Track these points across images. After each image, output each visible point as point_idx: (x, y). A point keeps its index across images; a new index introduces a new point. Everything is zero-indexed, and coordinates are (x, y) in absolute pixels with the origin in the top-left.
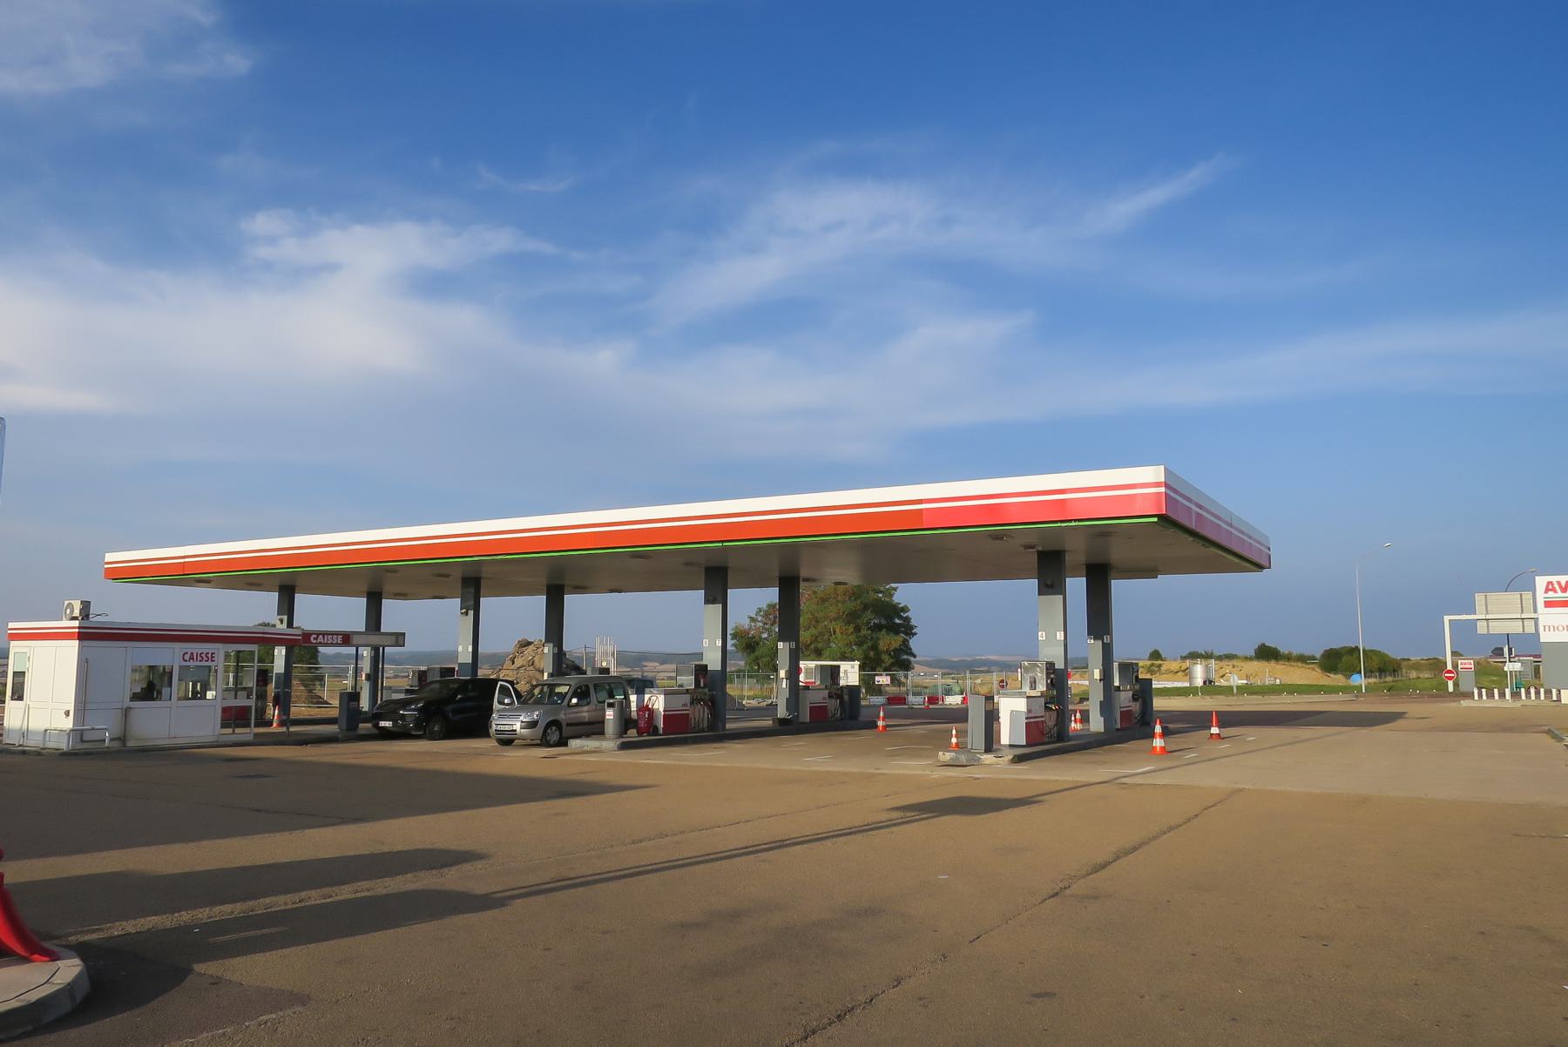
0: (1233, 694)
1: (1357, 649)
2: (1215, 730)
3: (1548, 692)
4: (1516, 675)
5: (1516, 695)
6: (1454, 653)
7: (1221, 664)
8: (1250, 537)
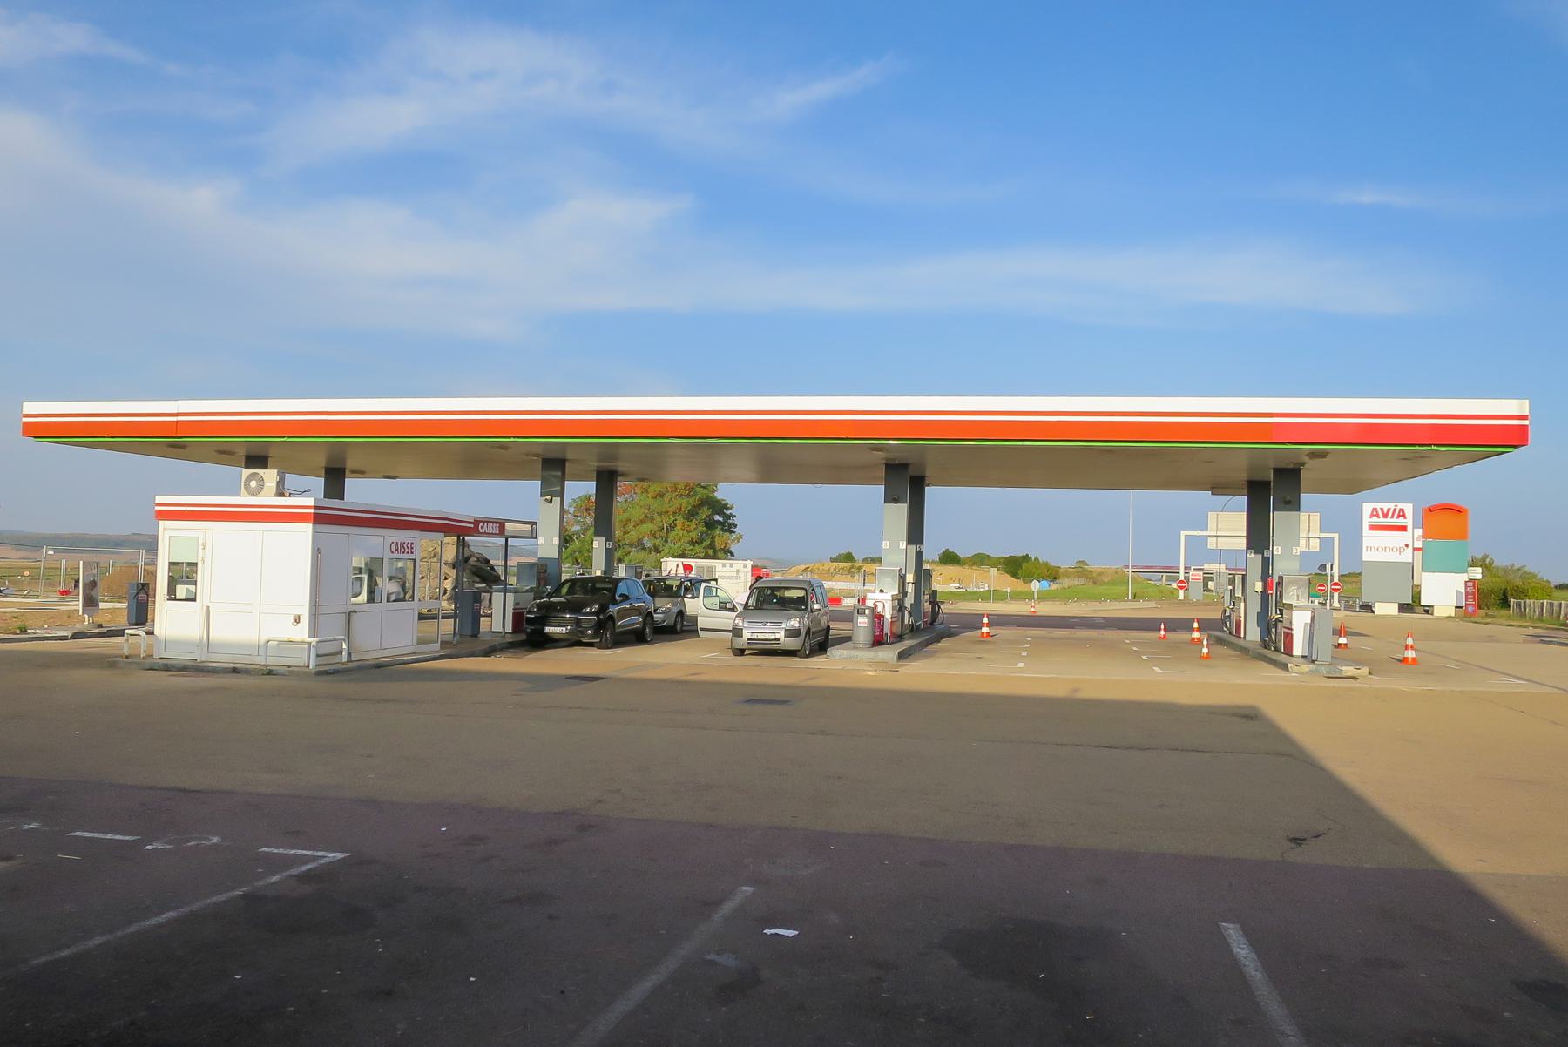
2: (985, 630)
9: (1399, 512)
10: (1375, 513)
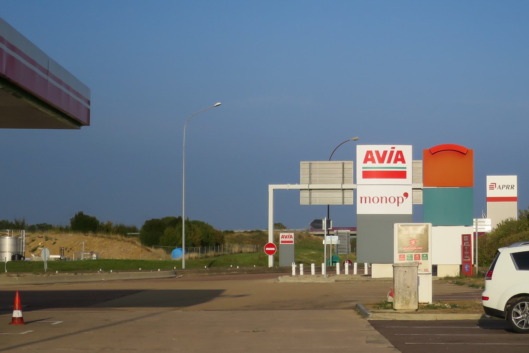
0: (43, 272)
1: (180, 219)
2: (17, 314)
3: (361, 267)
4: (333, 250)
5: (331, 270)
6: (278, 226)
7: (33, 236)
8: (68, 88)
9: (397, 156)
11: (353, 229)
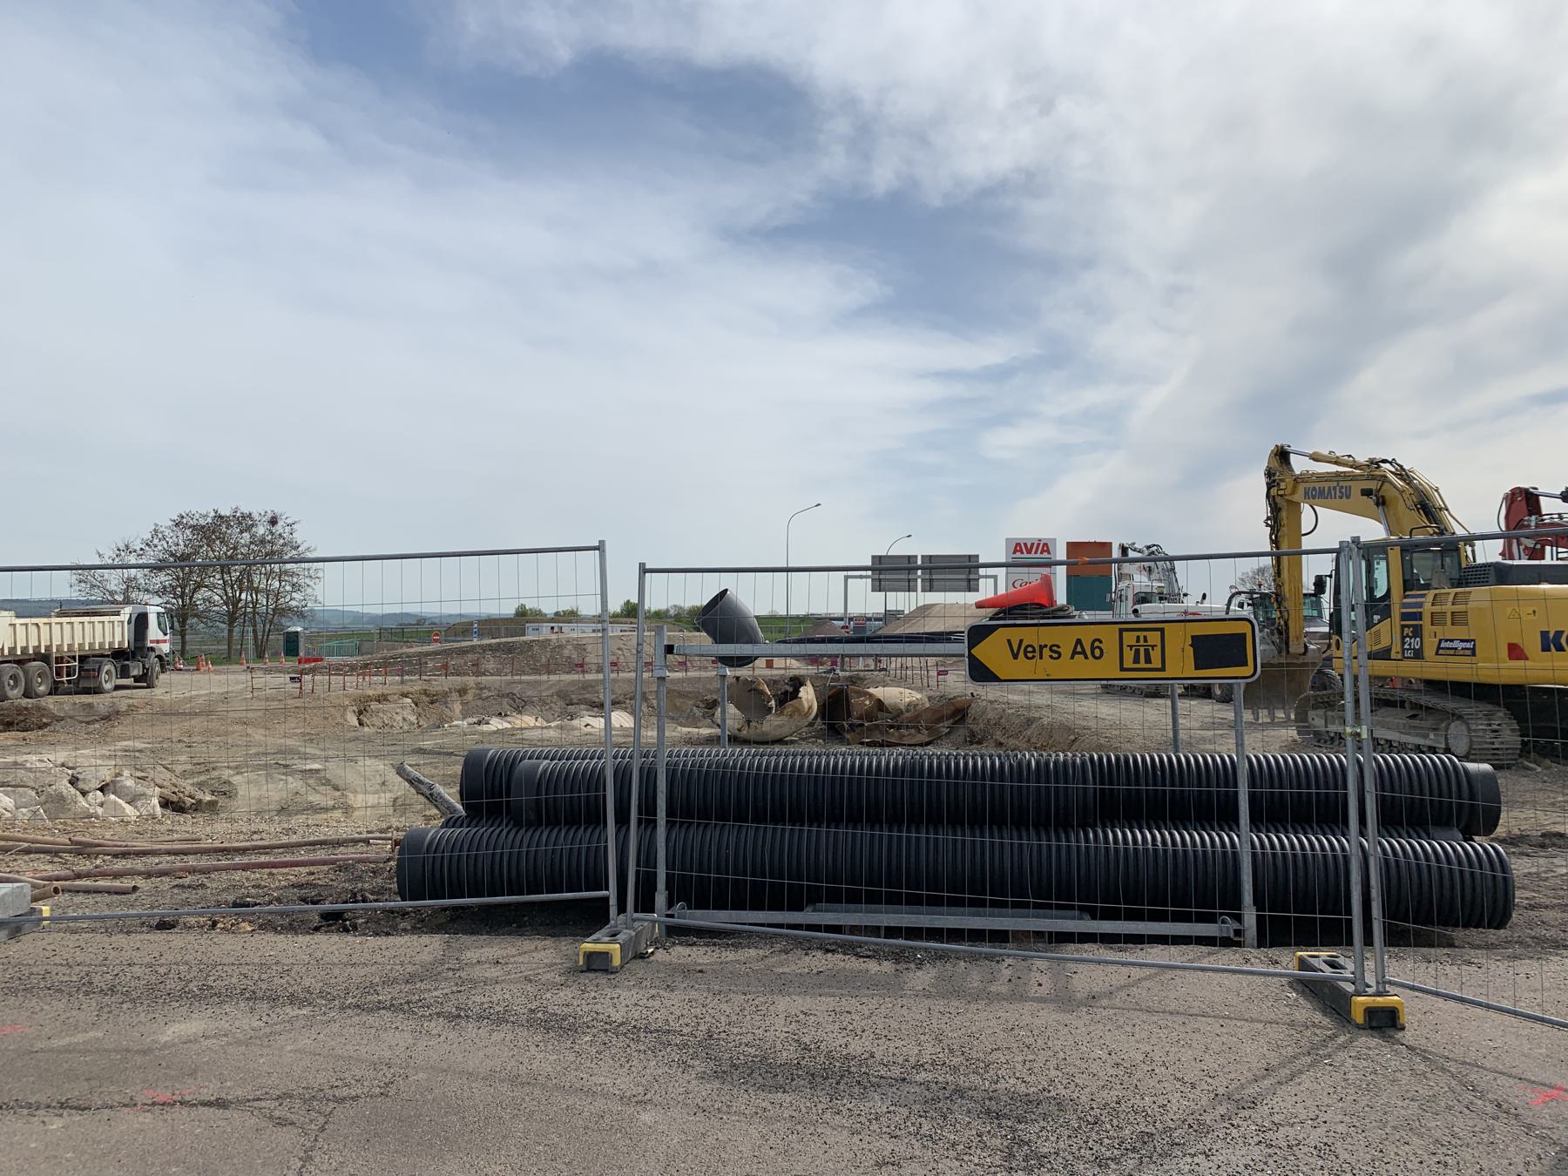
9: (1043, 548)
10: (1079, 649)
11: (930, 560)
